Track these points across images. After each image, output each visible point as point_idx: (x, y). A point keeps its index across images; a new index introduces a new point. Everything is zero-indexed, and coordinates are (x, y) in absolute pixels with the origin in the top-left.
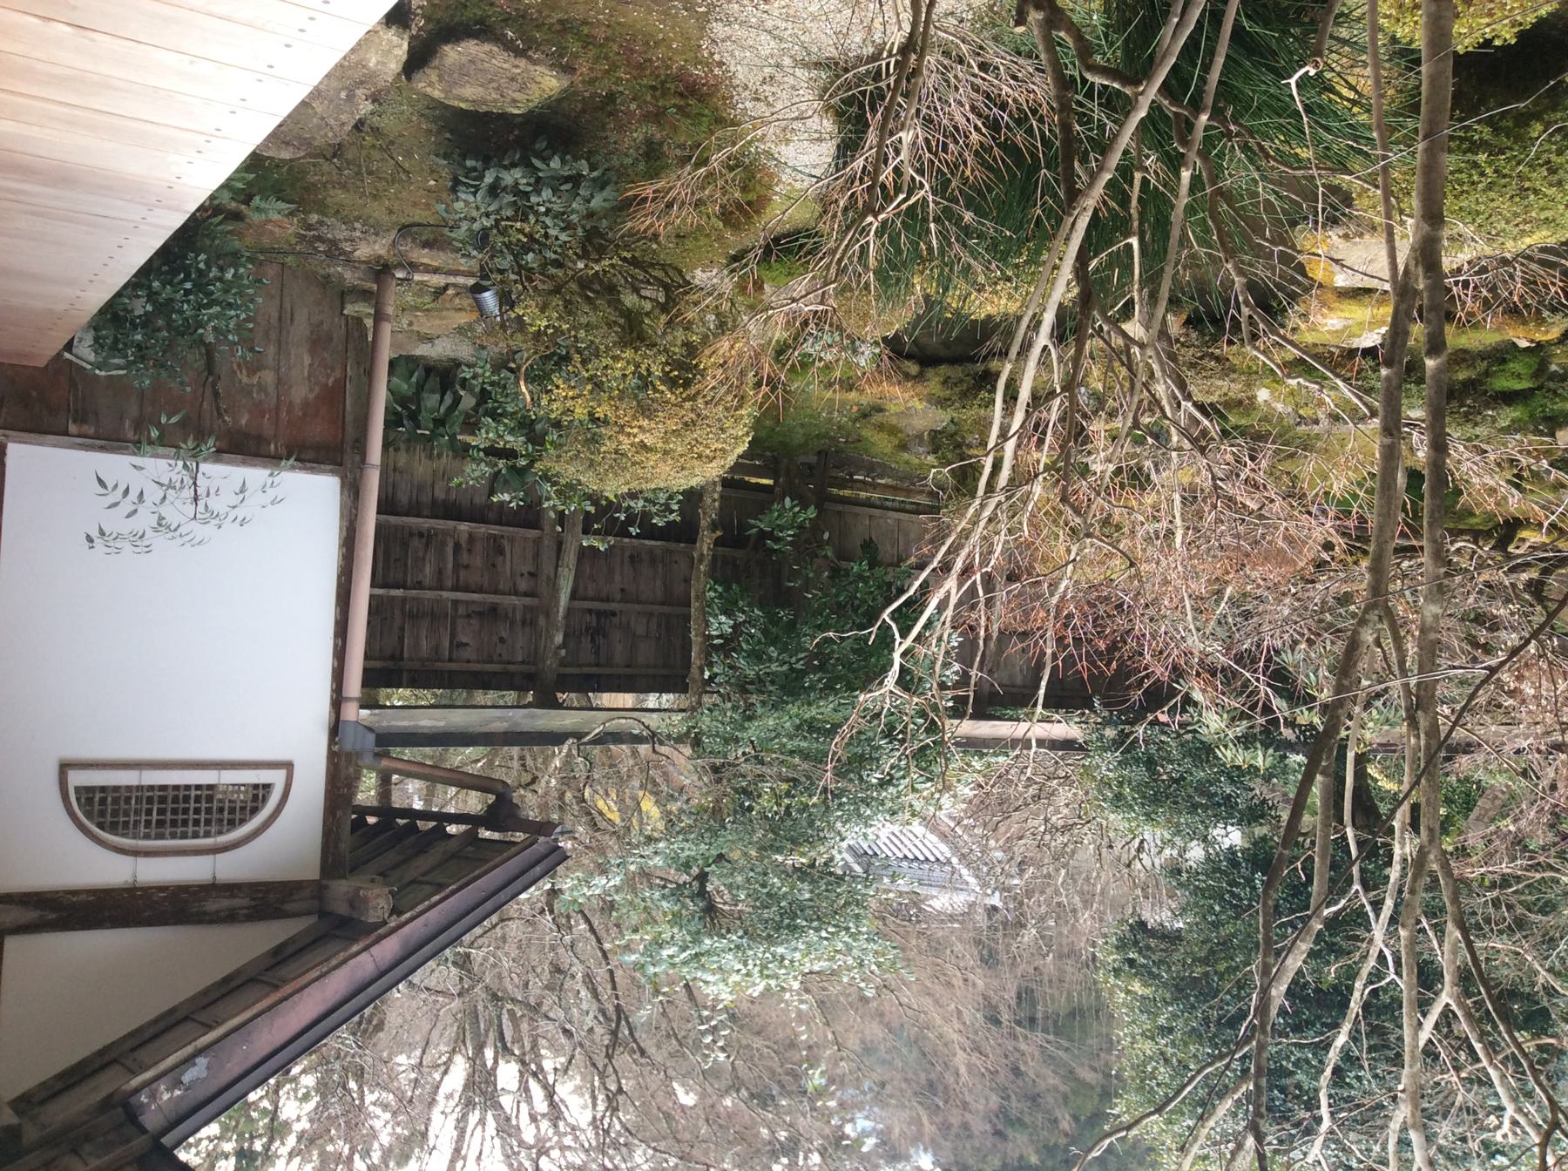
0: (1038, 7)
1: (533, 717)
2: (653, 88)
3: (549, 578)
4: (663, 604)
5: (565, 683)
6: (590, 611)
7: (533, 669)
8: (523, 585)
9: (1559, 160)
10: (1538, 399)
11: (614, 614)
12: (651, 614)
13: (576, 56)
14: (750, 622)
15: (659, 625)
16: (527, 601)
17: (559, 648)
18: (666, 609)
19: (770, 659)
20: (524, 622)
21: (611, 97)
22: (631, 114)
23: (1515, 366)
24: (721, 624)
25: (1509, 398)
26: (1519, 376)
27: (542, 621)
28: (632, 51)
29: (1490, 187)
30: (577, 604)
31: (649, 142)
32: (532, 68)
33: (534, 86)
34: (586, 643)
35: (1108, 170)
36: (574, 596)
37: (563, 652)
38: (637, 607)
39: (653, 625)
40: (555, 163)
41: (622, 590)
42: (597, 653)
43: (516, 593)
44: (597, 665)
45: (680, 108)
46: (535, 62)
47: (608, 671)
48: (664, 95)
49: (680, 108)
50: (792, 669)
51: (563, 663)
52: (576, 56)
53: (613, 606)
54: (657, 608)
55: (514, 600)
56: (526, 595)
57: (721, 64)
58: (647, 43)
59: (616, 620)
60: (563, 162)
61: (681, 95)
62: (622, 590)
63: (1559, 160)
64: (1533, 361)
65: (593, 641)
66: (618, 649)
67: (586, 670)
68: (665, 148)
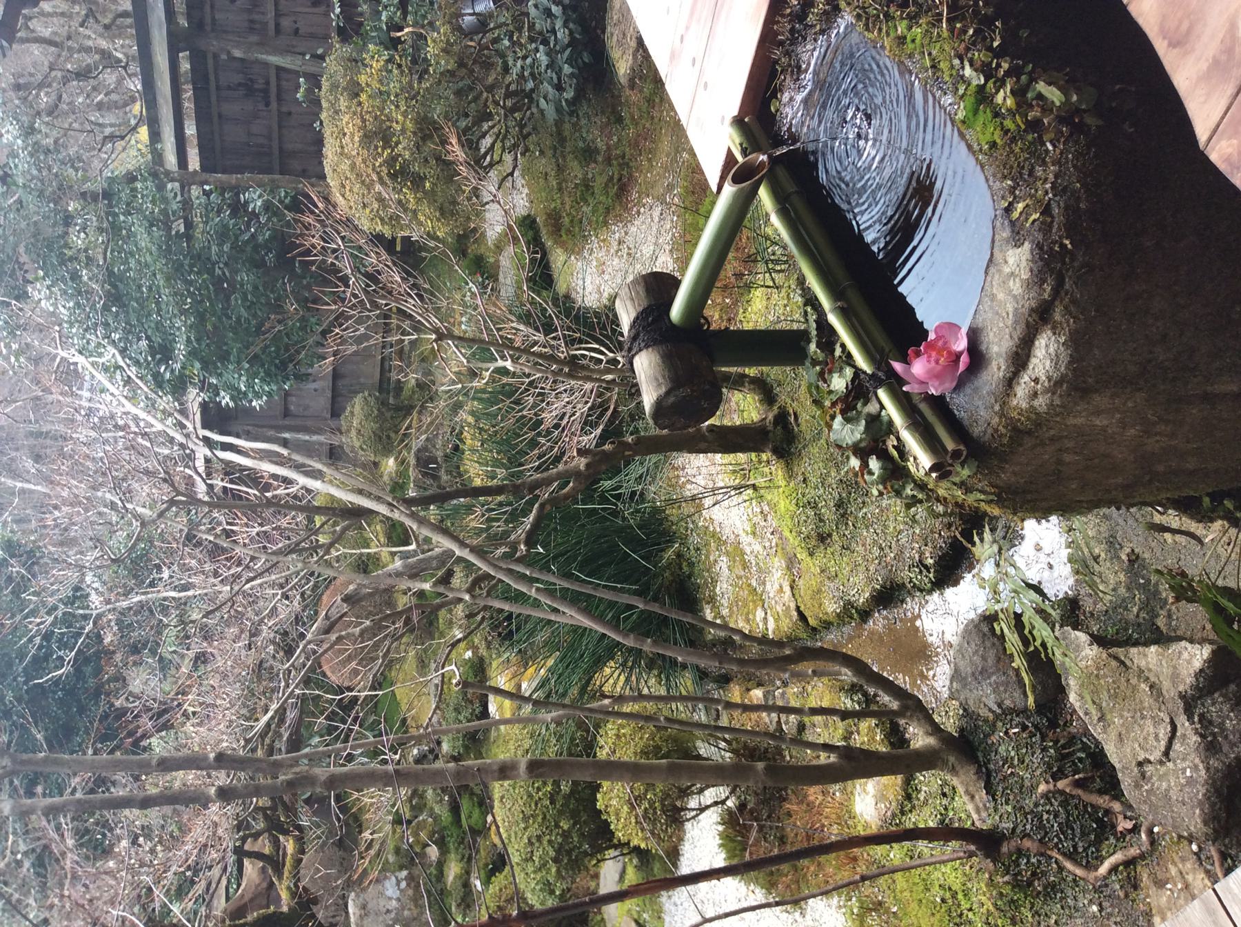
0: (588, 465)
1: (160, 26)
2: (623, 157)
3: (293, 47)
4: (281, 149)
5: (198, 59)
6: (268, 83)
7: (208, 28)
8: (286, 23)
9: (545, 843)
10: (455, 831)
11: (267, 104)
12: (270, 138)
13: (641, 91)
14: (260, 227)
15: (262, 146)
16: (272, 26)
17: (229, 53)
18: (276, 152)
19: (220, 245)
20: (252, 21)
21: (620, 120)
22: (610, 138)
23: (476, 813)
24: (255, 199)
25: (455, 809)
26: (470, 817)
27: (254, 38)
28: (646, 139)
29: (530, 796)
30: (273, 73)
31: (597, 151)
32: (631, 51)
33: (620, 53)
34: (237, 78)
35: (419, 528)
36: (279, 69)
37: (224, 57)
38: (275, 127)
39: (261, 140)
40: (567, 69)
41: (290, 113)
42: (229, 88)
43: (278, 15)
44: (218, 88)
45: (612, 178)
46: (634, 55)
47: (214, 99)
48: (620, 165)
49: (612, 178)
50: (214, 264)
51: (216, 56)
52: (641, 91)
53: (274, 105)
54: (275, 144)
55: (271, 15)
56: (277, 25)
57: (638, 213)
58: (650, 152)
59: (261, 106)
60: (572, 75)
61: (620, 179)
62: (290, 113)
63: (545, 843)
64: (479, 827)
65: (240, 84)
66: (233, 108)
67: (212, 77)
68: (593, 165)
